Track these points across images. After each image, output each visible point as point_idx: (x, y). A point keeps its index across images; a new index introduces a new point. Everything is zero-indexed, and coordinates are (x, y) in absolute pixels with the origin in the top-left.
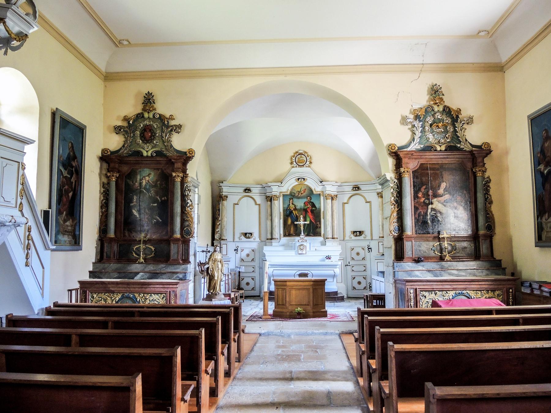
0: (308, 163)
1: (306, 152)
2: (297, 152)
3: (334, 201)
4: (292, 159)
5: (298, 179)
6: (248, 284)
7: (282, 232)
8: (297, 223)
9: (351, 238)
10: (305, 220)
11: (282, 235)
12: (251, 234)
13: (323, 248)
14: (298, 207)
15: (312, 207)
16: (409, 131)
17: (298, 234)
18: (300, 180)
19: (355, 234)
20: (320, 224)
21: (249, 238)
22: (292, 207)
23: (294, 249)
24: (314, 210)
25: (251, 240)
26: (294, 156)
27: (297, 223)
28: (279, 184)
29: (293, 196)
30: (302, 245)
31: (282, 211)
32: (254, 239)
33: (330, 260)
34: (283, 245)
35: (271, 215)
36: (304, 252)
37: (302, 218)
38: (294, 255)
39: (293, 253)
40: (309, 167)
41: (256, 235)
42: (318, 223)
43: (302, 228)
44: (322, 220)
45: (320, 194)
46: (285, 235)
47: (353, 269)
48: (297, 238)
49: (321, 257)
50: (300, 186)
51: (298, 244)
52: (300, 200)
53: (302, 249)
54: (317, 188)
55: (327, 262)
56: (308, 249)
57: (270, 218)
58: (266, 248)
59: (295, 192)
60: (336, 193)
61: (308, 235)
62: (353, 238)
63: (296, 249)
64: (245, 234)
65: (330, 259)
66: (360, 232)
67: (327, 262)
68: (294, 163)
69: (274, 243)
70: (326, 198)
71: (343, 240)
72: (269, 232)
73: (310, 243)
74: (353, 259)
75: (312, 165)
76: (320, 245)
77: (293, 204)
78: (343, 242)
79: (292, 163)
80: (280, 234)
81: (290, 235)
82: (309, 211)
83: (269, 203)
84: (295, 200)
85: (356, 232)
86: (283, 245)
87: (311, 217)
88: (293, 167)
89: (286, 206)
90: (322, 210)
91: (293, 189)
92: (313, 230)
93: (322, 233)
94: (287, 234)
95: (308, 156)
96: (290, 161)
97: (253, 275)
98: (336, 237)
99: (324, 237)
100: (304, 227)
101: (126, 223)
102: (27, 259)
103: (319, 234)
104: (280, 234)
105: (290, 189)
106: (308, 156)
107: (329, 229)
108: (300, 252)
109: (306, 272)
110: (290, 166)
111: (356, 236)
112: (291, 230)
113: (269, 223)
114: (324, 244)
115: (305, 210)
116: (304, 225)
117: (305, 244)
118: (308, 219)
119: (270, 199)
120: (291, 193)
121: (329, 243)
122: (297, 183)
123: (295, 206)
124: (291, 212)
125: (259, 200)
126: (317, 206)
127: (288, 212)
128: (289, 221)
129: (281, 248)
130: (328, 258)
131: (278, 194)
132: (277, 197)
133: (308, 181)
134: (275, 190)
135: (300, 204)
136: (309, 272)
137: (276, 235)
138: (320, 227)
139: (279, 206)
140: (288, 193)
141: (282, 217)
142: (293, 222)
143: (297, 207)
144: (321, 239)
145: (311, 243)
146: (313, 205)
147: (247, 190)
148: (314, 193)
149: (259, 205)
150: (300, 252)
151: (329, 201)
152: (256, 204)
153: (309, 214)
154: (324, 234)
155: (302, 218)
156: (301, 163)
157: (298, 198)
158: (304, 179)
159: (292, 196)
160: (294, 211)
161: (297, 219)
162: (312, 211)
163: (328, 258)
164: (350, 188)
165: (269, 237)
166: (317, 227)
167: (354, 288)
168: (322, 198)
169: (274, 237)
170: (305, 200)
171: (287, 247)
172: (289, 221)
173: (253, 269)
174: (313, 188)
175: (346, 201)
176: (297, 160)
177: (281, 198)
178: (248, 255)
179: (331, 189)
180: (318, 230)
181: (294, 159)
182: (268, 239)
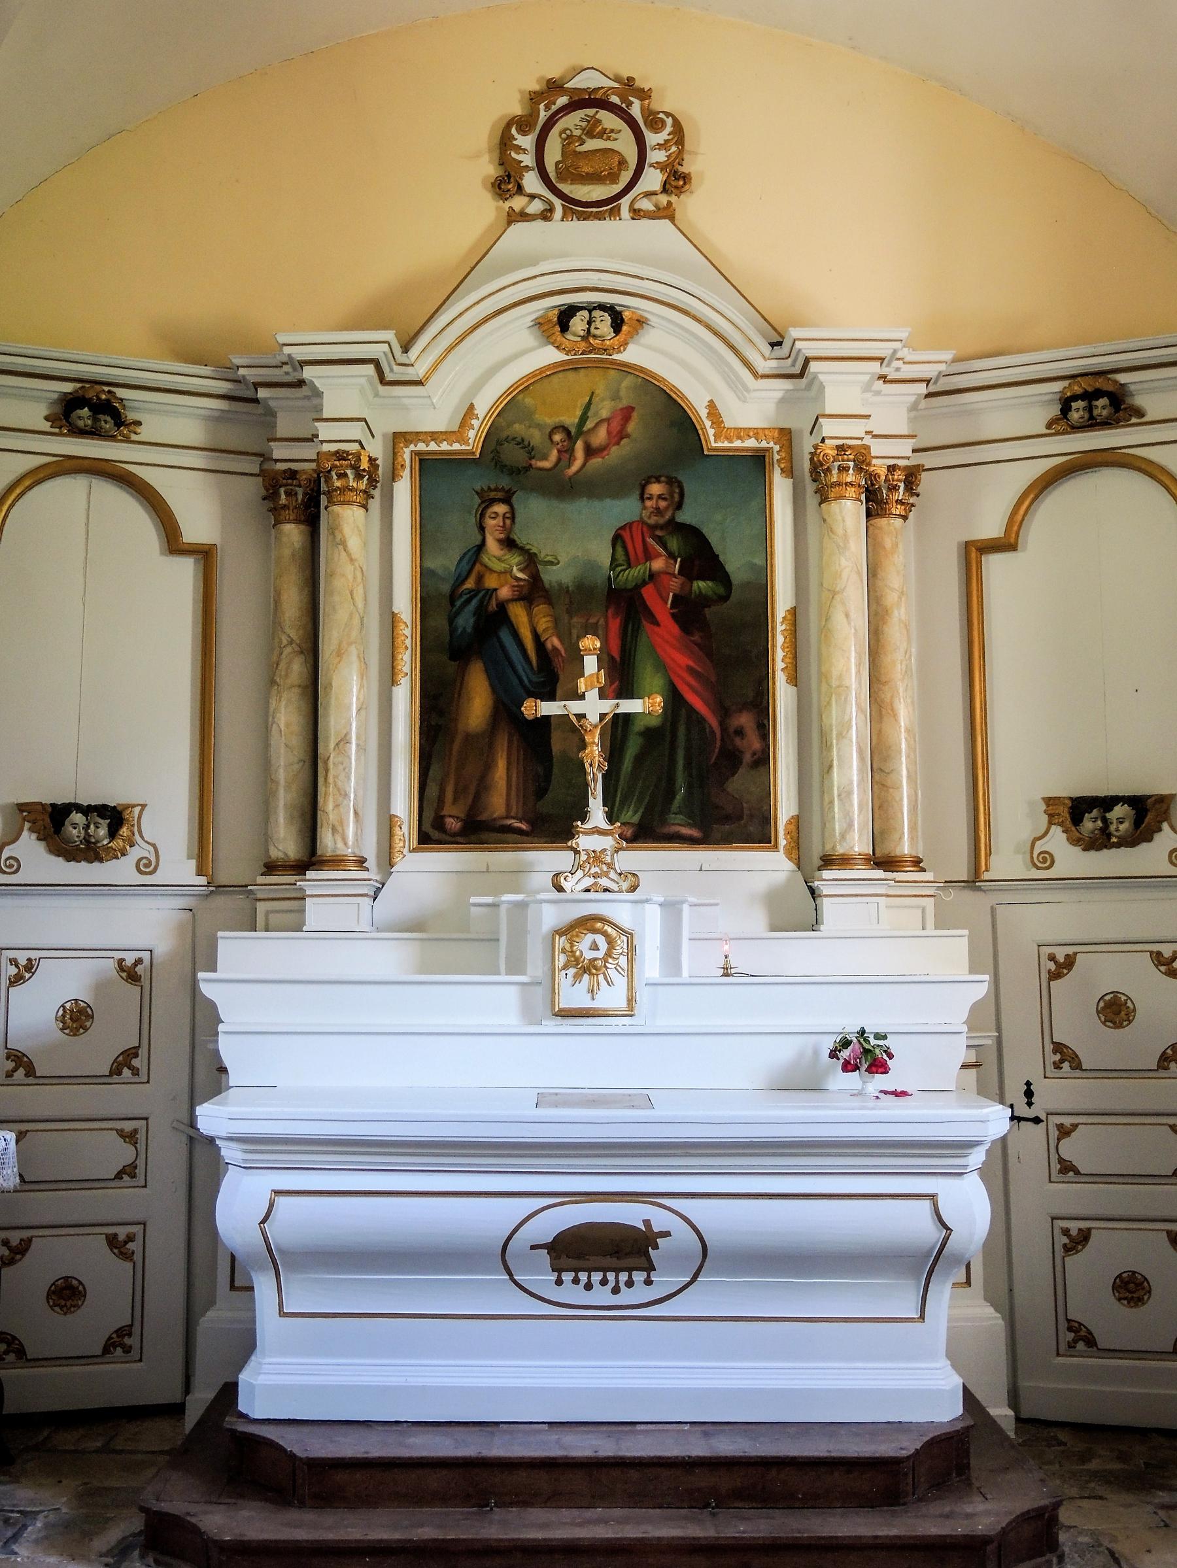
0: (652, 179)
1: (629, 86)
2: (554, 87)
3: (890, 525)
4: (505, 143)
5: (566, 315)
6: (67, 1294)
7: (403, 804)
8: (548, 708)
9: (1048, 860)
10: (621, 680)
11: (407, 830)
12: (115, 817)
13: (797, 953)
14: (556, 575)
15: (688, 572)
16: (919, 490)
17: (554, 825)
18: (578, 323)
19: (1089, 825)
20: (764, 727)
21: (90, 852)
22: (503, 571)
23: (516, 965)
24: (704, 601)
25: (120, 870)
26: (523, 124)
27: (548, 708)
28: (378, 342)
29: (517, 472)
30: (587, 923)
31: (404, 603)
32: (146, 867)
33: (879, 1082)
34: (414, 926)
35: (312, 648)
36: (612, 996)
37: (591, 664)
38: (512, 1019)
39: (496, 1001)
40: (666, 213)
41: (166, 825)
42: (745, 720)
43: (594, 754)
44: (783, 696)
45: (758, 461)
46: (431, 835)
47: (1069, 1149)
48: (547, 861)
49: (784, 1052)
50: (582, 383)
51: (551, 916)
52: (582, 510)
53: (588, 968)
54: (737, 405)
55: (850, 1106)
56: (650, 965)
57: (297, 668)
58: (238, 952)
59: (536, 438)
60: (901, 451)
61: (646, 832)
62: (1069, 858)
63: (536, 967)
64: (53, 822)
65: (878, 1066)
66: (1139, 804)
67: (850, 1106)
68: (532, 183)
69: (326, 901)
70: (819, 479)
71: (974, 881)
72: (286, 798)
73: (672, 909)
74: (1065, 1057)
75: (690, 205)
76: (757, 921)
77: (509, 543)
78: (968, 896)
79: (506, 183)
80: (388, 823)
81: (476, 831)
82: (662, 609)
83: (293, 533)
84: (534, 509)
85: (1107, 803)
86: (414, 926)
87: (681, 660)
88: (515, 217)
89: (447, 562)
90: (782, 600)
91: (513, 405)
92: (700, 782)
93: (785, 807)
94: (453, 816)
95: (655, 123)
96: (491, 170)
97: (122, 1203)
98: (905, 848)
99: (797, 852)
100: (614, 753)
101: (916, 824)
102: (266, 834)
103: (745, 825)
104: (388, 823)
105: (485, 403)
106: (655, 123)
107: (850, 772)
108: (573, 994)
109: (631, 1215)
110: (489, 208)
111: (1101, 841)
112: (492, 780)
113: (287, 716)
114: (799, 912)
115: (624, 606)
116: (618, 728)
117: (620, 911)
118: (651, 678)
119: (301, 500)
120: (495, 439)
121: (850, 902)
122: (551, 355)
123: (531, 561)
124: (494, 619)
125: (200, 512)
126: (735, 562)
127: (466, 621)
128: (477, 704)
129: (388, 957)
130: (865, 1056)
131: (376, 449)
132: (372, 480)
133: (649, 336)
134: (349, 411)
135: (577, 541)
136: (660, 1220)
137: (350, 826)
138: (763, 760)
139: (378, 560)
140: (473, 441)
141: (408, 661)
142: (505, 710)
143: (551, 576)
144: (768, 867)
145: (681, 906)
146: (701, 557)
147: (91, 408)
148: (713, 442)
149: (205, 555)
150: (573, 994)
151: (849, 512)
152: (173, 543)
153: (663, 635)
154: (798, 824)
155: (591, 664)
156: (594, 178)
157: (563, 488)
158: (618, 322)
159: (496, 471)
160: (518, 613)
161: (552, 678)
162: (689, 613)
163: (865, 1056)
164: (1031, 411)
165: (287, 845)
166: (731, 759)
167: (1081, 1337)
168: (781, 490)
169: (328, 843)
170: (626, 509)
171: (448, 942)
172: (477, 704)
173: (125, 1154)
174: (697, 400)
175: (991, 528)
176: (553, 153)
177: (403, 492)
178: (76, 1018)
179: (865, 412)
180: (740, 783)
181: (526, 141)
182: (271, 868)
